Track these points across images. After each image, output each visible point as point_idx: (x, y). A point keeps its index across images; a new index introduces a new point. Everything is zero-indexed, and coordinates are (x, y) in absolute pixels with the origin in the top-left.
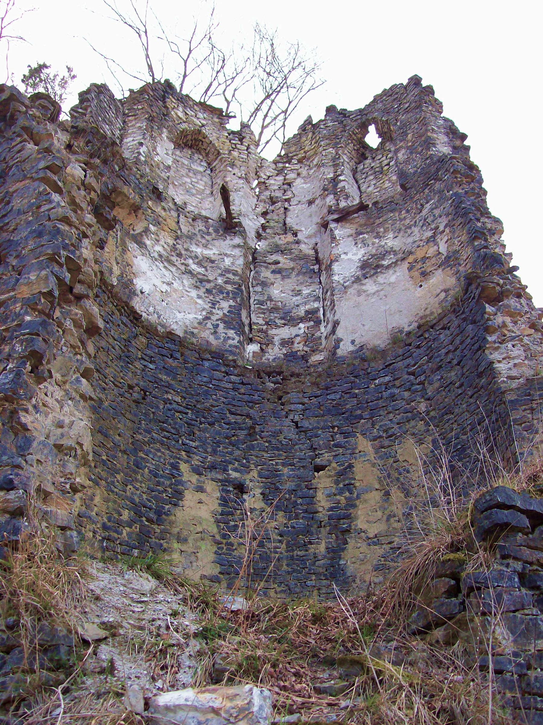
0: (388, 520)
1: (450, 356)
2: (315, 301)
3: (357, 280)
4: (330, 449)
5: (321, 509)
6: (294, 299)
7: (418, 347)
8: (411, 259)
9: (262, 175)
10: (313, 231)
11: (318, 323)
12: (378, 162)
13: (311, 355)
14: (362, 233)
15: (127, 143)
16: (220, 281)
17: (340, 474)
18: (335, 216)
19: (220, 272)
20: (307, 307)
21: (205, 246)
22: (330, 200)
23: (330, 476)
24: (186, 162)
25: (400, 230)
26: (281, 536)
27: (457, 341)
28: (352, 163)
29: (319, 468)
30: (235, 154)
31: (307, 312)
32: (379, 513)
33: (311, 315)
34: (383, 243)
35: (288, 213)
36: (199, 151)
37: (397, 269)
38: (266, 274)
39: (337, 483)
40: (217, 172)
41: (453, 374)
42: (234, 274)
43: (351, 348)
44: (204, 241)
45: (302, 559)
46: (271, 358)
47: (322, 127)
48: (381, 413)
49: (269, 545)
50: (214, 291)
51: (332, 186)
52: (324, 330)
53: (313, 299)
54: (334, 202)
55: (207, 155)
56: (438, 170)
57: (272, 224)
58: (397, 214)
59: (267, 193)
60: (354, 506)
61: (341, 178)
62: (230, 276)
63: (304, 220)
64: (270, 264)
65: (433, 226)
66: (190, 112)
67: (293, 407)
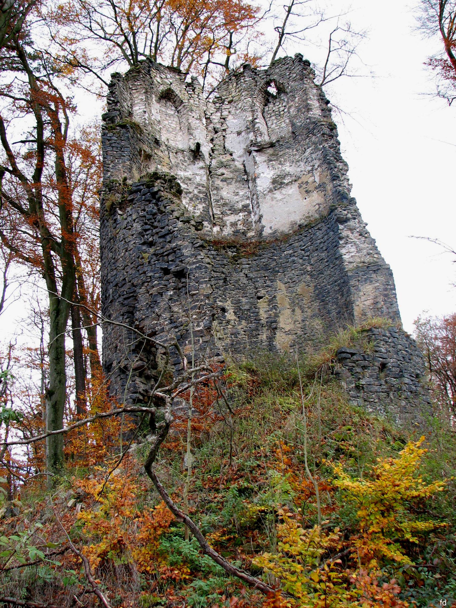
0: (294, 323)
1: (322, 245)
2: (247, 199)
3: (271, 191)
4: (264, 288)
5: (262, 318)
6: (235, 197)
7: (306, 236)
8: (300, 181)
9: (208, 113)
10: (242, 153)
11: (250, 213)
12: (277, 107)
13: (247, 233)
14: (271, 161)
15: (136, 111)
16: (196, 192)
17: (270, 301)
18: (256, 149)
19: (195, 186)
20: (243, 203)
21: (185, 170)
22: (251, 136)
23: (266, 302)
24: (164, 110)
25: (293, 162)
26: (245, 332)
27: (326, 238)
28: (262, 107)
29: (259, 298)
30: (191, 101)
31: (244, 206)
32: (290, 320)
33: (245, 207)
34: (284, 169)
35: (226, 140)
36: (169, 100)
37: (292, 186)
38: (218, 182)
39: (269, 305)
40: (182, 114)
41: (323, 254)
42: (202, 187)
43: (270, 231)
44: (184, 167)
45: (255, 342)
46: (226, 234)
47: (242, 81)
48: (288, 270)
49: (240, 337)
50: (194, 199)
51: (252, 126)
52: (253, 218)
53: (246, 198)
54: (254, 137)
55: (175, 102)
56: (314, 129)
57: (217, 147)
58: (291, 151)
59: (212, 125)
60: (278, 317)
61: (257, 121)
62: (201, 188)
63: (236, 145)
64: (219, 175)
65: (311, 164)
66: (163, 76)
67: (244, 266)
